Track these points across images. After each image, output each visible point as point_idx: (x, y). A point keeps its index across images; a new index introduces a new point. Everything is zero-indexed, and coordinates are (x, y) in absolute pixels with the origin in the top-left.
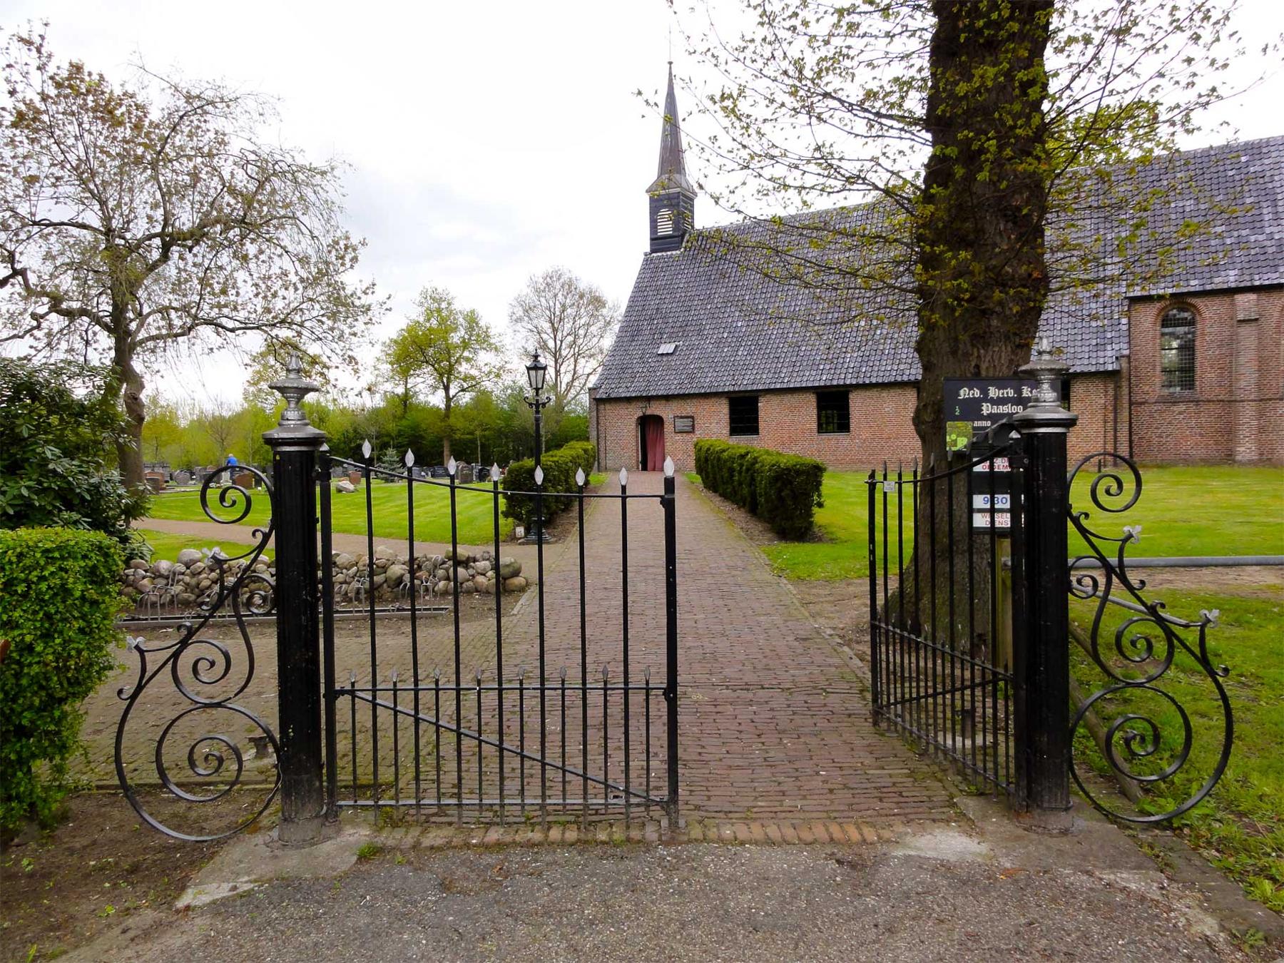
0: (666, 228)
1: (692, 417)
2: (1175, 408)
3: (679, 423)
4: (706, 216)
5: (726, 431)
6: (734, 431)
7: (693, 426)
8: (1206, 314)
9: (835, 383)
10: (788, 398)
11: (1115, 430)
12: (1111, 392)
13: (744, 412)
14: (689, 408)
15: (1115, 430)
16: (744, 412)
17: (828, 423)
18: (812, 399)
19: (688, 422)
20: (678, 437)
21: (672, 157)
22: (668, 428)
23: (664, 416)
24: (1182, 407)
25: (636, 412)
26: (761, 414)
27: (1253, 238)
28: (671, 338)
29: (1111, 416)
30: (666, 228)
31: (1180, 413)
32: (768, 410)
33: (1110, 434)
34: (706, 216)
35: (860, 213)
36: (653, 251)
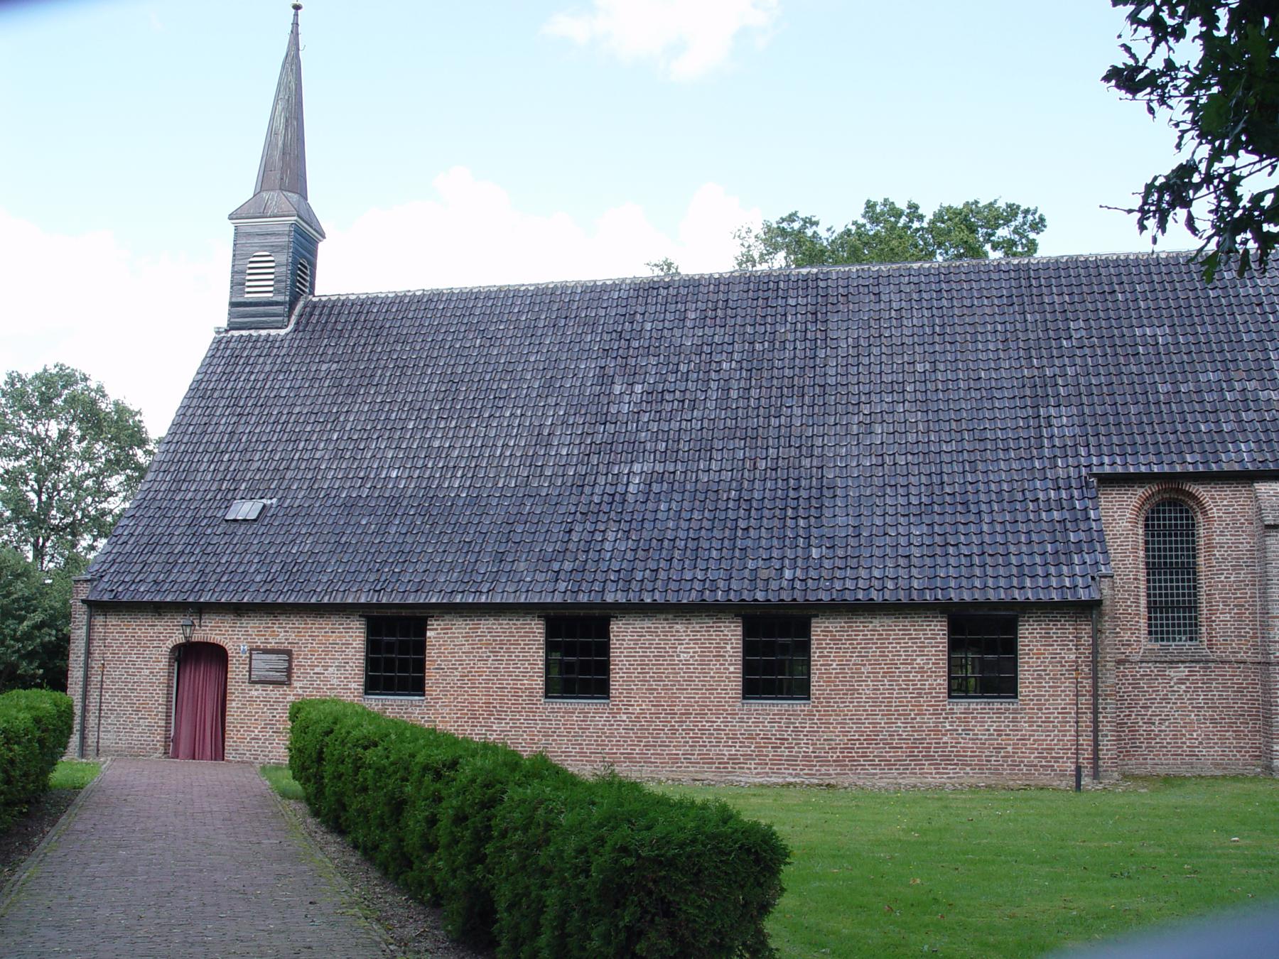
0: (262, 288)
1: (289, 653)
2: (1171, 673)
3: (260, 662)
4: (336, 277)
5: (357, 684)
6: (373, 685)
7: (289, 671)
8: (1214, 513)
9: (583, 598)
10: (488, 626)
11: (1095, 712)
12: (1086, 640)
13: (396, 654)
14: (282, 632)
15: (1095, 712)
16: (396, 654)
17: (404, 666)
18: (537, 629)
19: (278, 661)
20: (256, 692)
21: (286, 164)
22: (237, 672)
23: (229, 646)
24: (1183, 670)
25: (171, 633)
26: (431, 654)
27: (1263, 395)
28: (251, 495)
29: (1087, 683)
30: (262, 288)
31: (1181, 681)
32: (445, 643)
33: (1087, 718)
34: (336, 277)
35: (624, 294)
36: (232, 327)
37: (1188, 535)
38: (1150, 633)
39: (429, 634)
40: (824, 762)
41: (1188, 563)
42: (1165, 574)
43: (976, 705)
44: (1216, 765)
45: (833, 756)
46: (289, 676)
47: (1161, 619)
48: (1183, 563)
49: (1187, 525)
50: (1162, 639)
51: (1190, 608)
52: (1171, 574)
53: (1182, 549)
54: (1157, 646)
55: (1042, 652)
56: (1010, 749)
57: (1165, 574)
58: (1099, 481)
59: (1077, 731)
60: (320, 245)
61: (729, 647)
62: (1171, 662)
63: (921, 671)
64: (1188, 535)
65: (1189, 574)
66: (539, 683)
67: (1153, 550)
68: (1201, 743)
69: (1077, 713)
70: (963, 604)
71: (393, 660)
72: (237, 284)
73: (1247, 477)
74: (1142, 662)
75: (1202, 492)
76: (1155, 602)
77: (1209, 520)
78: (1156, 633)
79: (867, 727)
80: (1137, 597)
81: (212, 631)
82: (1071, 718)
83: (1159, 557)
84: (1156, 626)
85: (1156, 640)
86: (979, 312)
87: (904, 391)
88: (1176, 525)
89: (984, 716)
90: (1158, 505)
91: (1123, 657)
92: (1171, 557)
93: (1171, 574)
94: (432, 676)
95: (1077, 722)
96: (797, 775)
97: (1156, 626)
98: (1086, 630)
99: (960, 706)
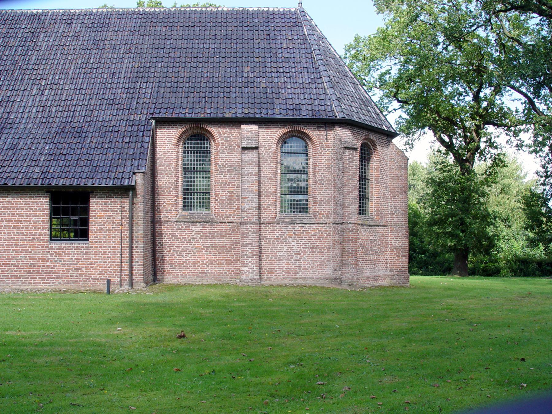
2: (193, 228)
8: (219, 141)
12: (127, 208)
24: (199, 226)
29: (127, 233)
31: (198, 233)
33: (126, 253)
38: (184, 206)
43: (65, 244)
44: (215, 278)
47: (191, 198)
50: (191, 210)
54: (187, 213)
55: (103, 213)
56: (84, 269)
58: (156, 122)
59: (121, 260)
62: (193, 222)
63: (35, 225)
68: (208, 266)
69: (121, 249)
70: (57, 187)
73: (236, 122)
74: (177, 222)
75: (214, 130)
76: (188, 189)
77: (217, 145)
78: (188, 206)
80: (177, 186)
83: (191, 165)
84: (188, 202)
85: (188, 210)
86: (229, 60)
87: (261, 113)
88: (201, 148)
89: (71, 249)
90: (192, 136)
92: (197, 165)
95: (121, 255)
97: (188, 202)
98: (127, 202)
99: (57, 245)
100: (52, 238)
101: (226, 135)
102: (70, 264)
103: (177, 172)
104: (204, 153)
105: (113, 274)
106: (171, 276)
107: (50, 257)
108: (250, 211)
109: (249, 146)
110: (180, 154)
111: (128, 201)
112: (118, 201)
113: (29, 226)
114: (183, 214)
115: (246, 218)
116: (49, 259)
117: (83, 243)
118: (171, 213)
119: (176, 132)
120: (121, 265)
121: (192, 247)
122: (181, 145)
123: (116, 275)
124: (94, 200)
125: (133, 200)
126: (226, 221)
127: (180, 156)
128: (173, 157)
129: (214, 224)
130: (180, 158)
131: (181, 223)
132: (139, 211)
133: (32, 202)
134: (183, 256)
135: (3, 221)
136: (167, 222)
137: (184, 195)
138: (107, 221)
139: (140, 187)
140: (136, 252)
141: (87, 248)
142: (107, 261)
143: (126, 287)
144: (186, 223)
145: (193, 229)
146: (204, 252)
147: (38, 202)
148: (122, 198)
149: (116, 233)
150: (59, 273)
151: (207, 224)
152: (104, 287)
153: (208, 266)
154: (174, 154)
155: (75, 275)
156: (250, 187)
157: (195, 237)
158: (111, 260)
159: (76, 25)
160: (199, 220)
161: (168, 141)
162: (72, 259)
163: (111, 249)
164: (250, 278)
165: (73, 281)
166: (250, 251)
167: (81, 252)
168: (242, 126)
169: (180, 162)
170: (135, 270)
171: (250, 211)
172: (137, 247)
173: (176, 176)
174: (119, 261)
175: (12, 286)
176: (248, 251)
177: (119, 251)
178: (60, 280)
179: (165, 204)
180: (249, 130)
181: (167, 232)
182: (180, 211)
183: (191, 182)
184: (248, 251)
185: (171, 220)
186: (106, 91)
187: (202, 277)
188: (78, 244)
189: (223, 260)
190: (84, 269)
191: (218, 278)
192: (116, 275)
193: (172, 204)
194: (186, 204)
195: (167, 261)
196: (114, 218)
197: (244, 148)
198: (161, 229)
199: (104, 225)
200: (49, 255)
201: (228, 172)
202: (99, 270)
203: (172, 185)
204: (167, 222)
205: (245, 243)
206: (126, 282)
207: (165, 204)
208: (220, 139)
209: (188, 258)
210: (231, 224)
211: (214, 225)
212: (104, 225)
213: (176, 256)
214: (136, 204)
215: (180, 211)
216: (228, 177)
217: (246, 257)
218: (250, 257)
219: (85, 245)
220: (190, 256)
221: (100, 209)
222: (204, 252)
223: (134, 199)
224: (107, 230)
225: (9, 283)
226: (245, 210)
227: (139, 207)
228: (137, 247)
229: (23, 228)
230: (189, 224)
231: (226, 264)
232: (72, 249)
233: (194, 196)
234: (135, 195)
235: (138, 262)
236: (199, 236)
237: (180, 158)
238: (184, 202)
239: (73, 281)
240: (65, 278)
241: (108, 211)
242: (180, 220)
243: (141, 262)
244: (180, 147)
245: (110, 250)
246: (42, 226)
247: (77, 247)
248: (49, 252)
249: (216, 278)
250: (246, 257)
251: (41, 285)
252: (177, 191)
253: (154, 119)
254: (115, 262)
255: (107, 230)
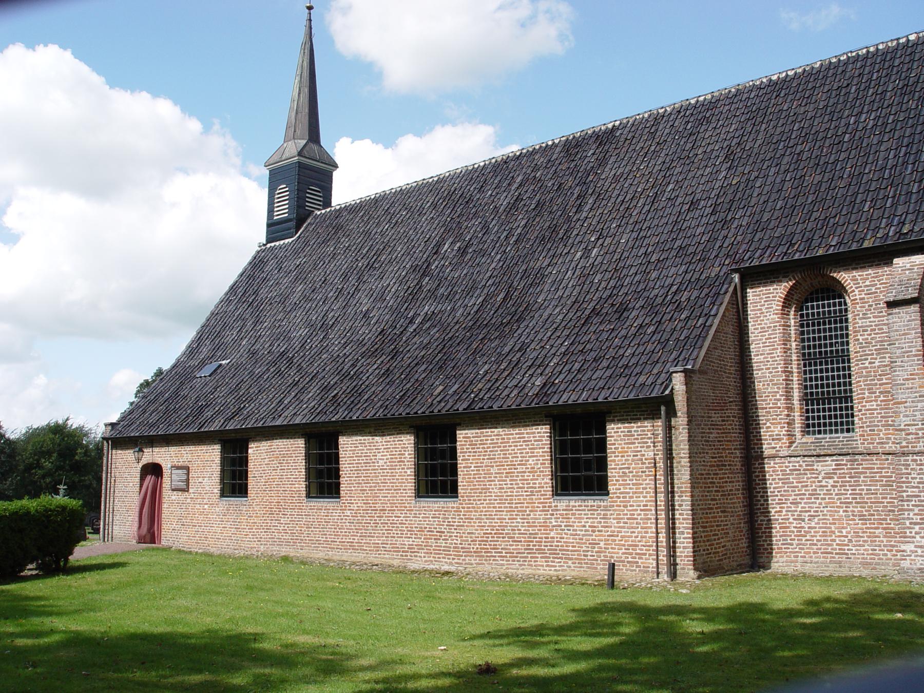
0: (282, 211)
2: (818, 466)
31: (829, 476)
36: (269, 241)
37: (841, 322)
38: (808, 426)
39: (250, 451)
40: (468, 552)
41: (843, 350)
42: (821, 364)
44: (865, 564)
45: (474, 547)
46: (188, 485)
48: (837, 351)
49: (840, 311)
51: (846, 398)
52: (827, 364)
53: (836, 336)
54: (810, 439)
55: (630, 447)
56: (602, 544)
57: (821, 364)
60: (335, 173)
61: (407, 453)
62: (818, 456)
64: (841, 322)
65: (843, 362)
66: (302, 486)
67: (809, 340)
68: (850, 541)
71: (590, 477)
72: (271, 211)
73: (881, 256)
74: (791, 457)
75: (845, 277)
79: (496, 523)
81: (152, 455)
82: (651, 515)
88: (829, 312)
90: (817, 292)
91: (774, 452)
93: (827, 364)
94: (252, 484)
96: (451, 564)
100: (223, 494)
101: (868, 283)
102: (583, 535)
103: (787, 362)
104: (836, 322)
105: (645, 554)
106: (785, 559)
107: (554, 524)
108: (912, 429)
109: (900, 297)
110: (792, 328)
111: (660, 424)
112: (648, 424)
113: (525, 472)
114: (804, 440)
115: (904, 444)
116: (554, 526)
117: (575, 500)
118: (779, 440)
119: (778, 290)
120: (657, 537)
121: (820, 504)
122: (792, 313)
123: (650, 555)
124: (613, 426)
125: (670, 421)
126: (880, 450)
127: (793, 332)
128: (778, 336)
129: (857, 457)
130: (793, 336)
131: (799, 459)
132: (682, 441)
133: (527, 433)
134: (803, 520)
135: (493, 466)
136: (773, 457)
137: (807, 405)
138: (633, 460)
139: (680, 398)
140: (680, 514)
141: (606, 508)
142: (636, 530)
143: (665, 577)
144: (806, 459)
145: (820, 468)
146: (841, 513)
147: (534, 433)
148: (653, 419)
149: (647, 482)
150: (568, 550)
151: (845, 458)
152: (604, 574)
153: (850, 541)
154: (779, 330)
155: (590, 553)
156: (908, 379)
157: (824, 483)
158: (642, 528)
159: (664, 130)
160: (829, 452)
161: (766, 305)
162: (584, 526)
163: (641, 510)
164: (919, 566)
165: (587, 563)
166: (916, 511)
167: (598, 514)
168: (896, 261)
169: (794, 344)
170: (679, 547)
171: (912, 429)
172: (680, 505)
173: (785, 372)
174: (654, 530)
175: (507, 568)
176: (911, 510)
177: (654, 512)
178: (570, 562)
179: (768, 424)
180: (908, 266)
181: (777, 476)
182: (798, 435)
183: (844, 376)
184: (911, 510)
185: (781, 454)
186: (893, 219)
187: (840, 562)
188: (592, 502)
189: (878, 528)
190: (602, 544)
191: (870, 564)
192: (650, 555)
193: (780, 423)
194: (811, 422)
195: (776, 531)
196: (644, 455)
197: (891, 305)
198: (763, 471)
199: (629, 468)
200: (553, 520)
201: (878, 354)
202: (624, 545)
203: (778, 388)
204: (773, 457)
205: (905, 494)
206: (664, 569)
207: (768, 424)
208: (857, 292)
209: (813, 525)
210: (890, 457)
211: (856, 460)
212: (629, 468)
213: (791, 520)
214: (676, 429)
215: (798, 435)
216: (877, 364)
217: (908, 522)
218: (916, 524)
219: (602, 504)
220: (816, 520)
221: (621, 440)
222: (841, 513)
223: (673, 420)
224: (633, 476)
225: (503, 565)
226: (902, 427)
227: (680, 433)
228: (680, 505)
229: (517, 476)
230: (813, 459)
231: (885, 537)
232: (584, 510)
233: (828, 402)
234: (672, 412)
235: (683, 533)
236: (831, 481)
237: (793, 336)
238: (808, 418)
239: (587, 563)
240: (576, 559)
241: (634, 443)
242: (796, 453)
243: (688, 533)
244: (792, 317)
245: (639, 512)
246: (542, 472)
247: (592, 506)
248: (553, 515)
249: (867, 564)
250: (908, 522)
251: (544, 569)
252: (788, 397)
253: (735, 271)
254: (647, 532)
255: (633, 476)
